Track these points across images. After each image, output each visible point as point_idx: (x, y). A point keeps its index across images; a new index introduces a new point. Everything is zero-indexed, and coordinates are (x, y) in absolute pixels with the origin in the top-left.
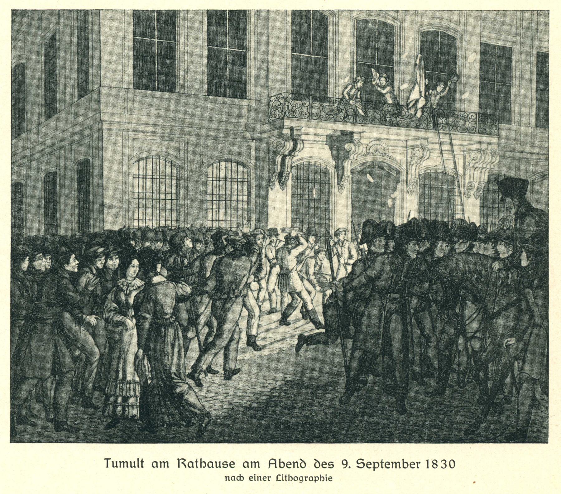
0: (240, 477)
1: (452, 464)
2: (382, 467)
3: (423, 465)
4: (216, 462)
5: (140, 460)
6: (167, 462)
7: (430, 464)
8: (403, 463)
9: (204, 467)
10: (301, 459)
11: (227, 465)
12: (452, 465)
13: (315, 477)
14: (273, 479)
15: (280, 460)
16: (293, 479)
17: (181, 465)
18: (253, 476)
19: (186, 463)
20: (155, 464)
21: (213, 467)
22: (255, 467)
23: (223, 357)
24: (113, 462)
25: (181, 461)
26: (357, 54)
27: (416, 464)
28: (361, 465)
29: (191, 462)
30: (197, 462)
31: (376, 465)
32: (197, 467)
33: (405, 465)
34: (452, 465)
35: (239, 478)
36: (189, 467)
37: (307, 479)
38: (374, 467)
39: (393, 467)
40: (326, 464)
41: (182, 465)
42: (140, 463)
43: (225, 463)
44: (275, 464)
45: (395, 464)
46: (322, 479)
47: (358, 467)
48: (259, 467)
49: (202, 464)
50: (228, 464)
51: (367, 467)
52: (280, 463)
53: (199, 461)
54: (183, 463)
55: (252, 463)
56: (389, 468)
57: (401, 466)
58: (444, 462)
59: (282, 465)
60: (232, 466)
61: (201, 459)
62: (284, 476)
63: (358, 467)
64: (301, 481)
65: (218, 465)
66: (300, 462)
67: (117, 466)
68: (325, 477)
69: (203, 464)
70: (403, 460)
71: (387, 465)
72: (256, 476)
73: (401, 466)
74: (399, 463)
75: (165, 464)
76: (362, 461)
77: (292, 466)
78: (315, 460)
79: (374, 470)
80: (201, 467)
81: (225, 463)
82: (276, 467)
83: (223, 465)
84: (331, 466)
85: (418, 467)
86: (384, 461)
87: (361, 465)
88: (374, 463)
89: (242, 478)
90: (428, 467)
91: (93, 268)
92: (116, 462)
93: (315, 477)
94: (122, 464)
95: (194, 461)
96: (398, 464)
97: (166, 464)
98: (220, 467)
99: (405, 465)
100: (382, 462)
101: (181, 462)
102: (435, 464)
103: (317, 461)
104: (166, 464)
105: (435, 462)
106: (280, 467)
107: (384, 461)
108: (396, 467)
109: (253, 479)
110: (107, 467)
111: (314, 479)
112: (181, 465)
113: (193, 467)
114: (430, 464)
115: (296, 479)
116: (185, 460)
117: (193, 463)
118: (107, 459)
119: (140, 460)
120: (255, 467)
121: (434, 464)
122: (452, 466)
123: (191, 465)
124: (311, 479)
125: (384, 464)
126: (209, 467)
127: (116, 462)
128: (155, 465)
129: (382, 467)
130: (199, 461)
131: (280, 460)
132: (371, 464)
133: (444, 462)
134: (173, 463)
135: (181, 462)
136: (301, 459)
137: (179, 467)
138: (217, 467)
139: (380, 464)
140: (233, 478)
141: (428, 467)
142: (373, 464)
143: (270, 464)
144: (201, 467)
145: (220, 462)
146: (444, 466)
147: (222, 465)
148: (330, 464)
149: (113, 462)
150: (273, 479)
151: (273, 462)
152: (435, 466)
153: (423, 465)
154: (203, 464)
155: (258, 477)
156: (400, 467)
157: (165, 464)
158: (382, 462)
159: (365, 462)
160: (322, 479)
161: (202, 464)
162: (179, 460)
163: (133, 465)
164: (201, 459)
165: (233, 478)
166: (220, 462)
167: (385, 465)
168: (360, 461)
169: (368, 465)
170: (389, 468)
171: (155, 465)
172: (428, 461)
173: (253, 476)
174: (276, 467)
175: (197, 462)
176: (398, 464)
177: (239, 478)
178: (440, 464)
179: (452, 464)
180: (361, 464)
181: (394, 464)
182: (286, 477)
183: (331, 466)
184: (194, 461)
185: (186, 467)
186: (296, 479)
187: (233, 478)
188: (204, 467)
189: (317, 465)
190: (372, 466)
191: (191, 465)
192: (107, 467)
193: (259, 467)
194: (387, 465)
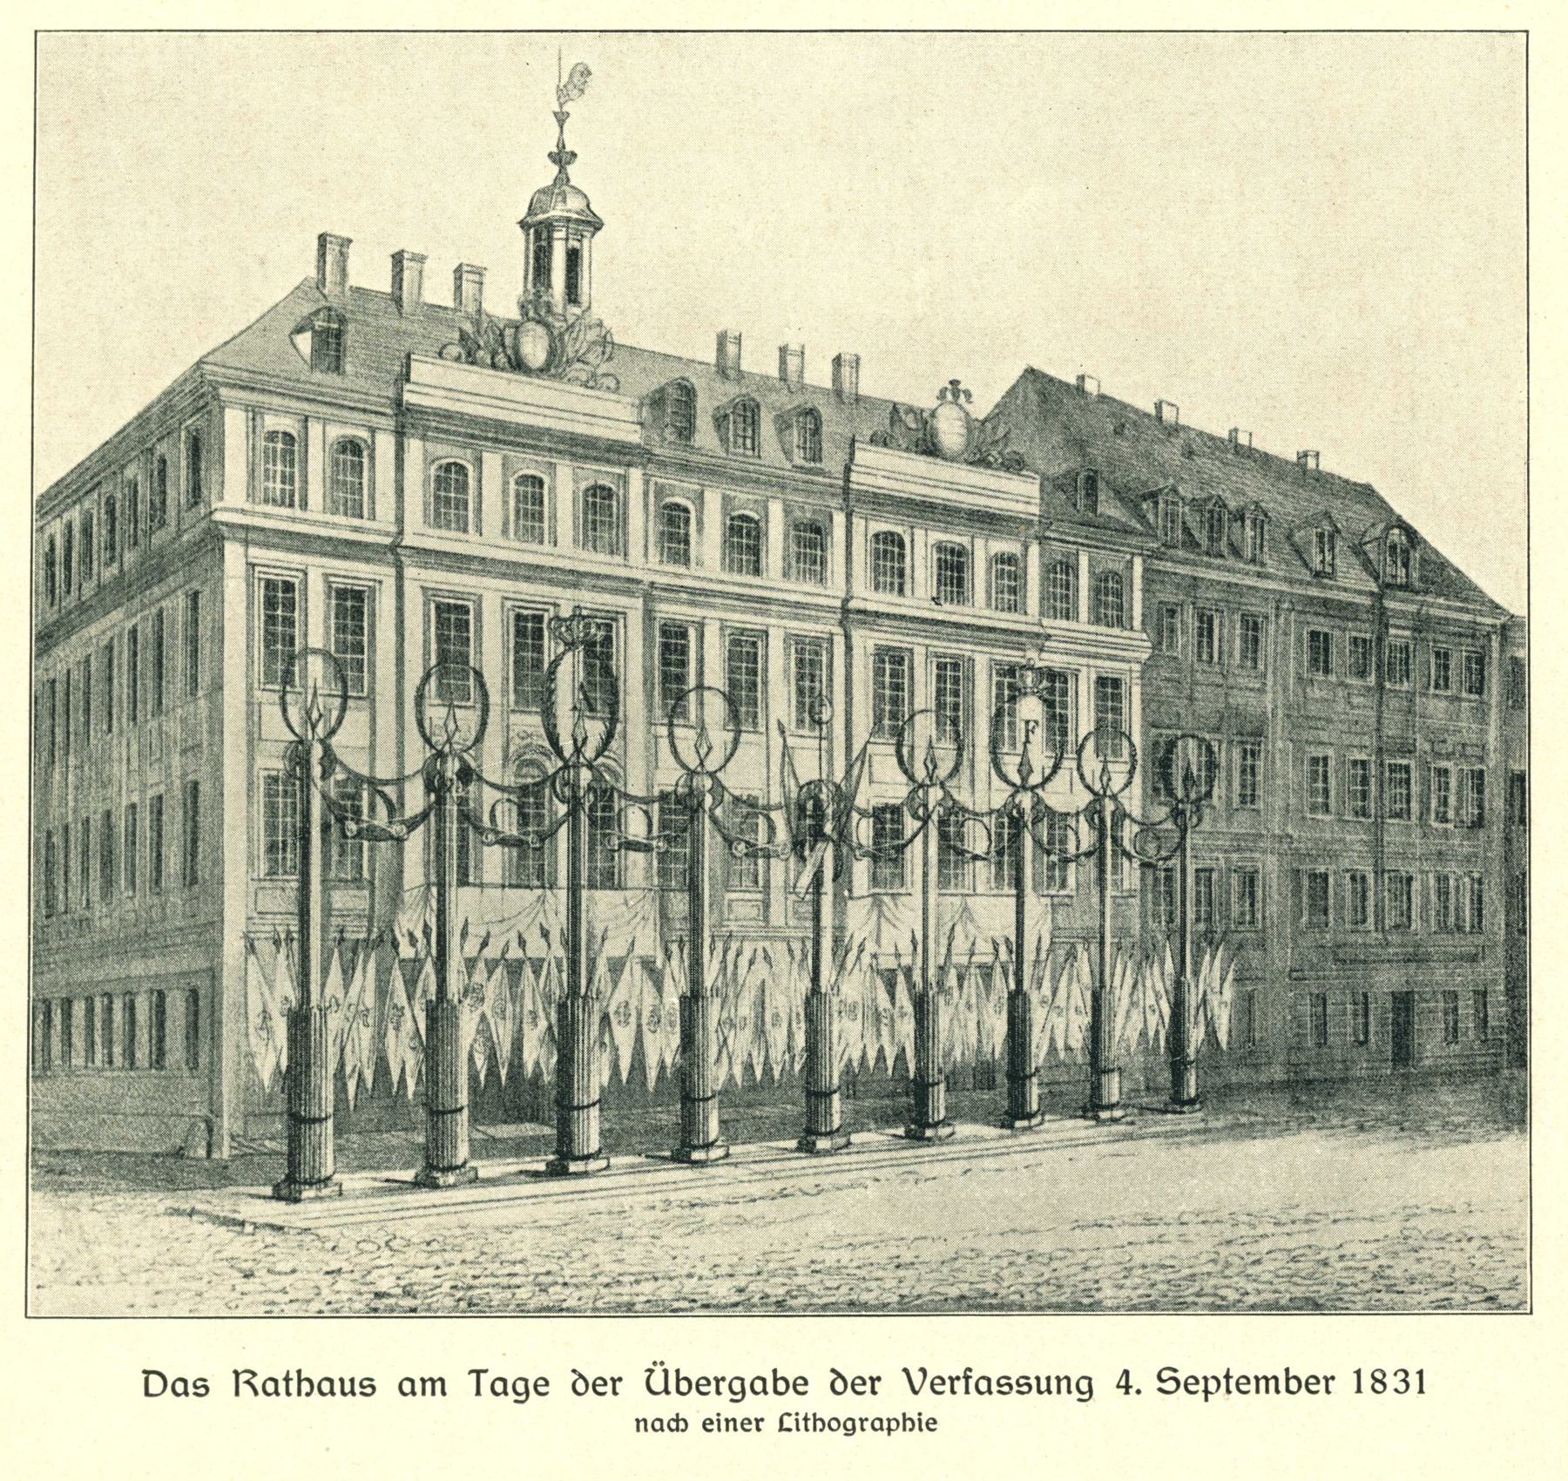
0: (677, 1420)
1: (1414, 1381)
6: (442, 1380)
7: (1367, 1382)
8: (1288, 1380)
9: (308, 1394)
13: (889, 1420)
14: (770, 1425)
15: (678, 1371)
16: (827, 1425)
17: (244, 1388)
18: (714, 1418)
19: (258, 1382)
20: (407, 1387)
22: (1267, 1391)
24: (666, 1372)
25: (244, 1377)
27: (713, 1383)
28: (1171, 1385)
30: (287, 1379)
31: (1212, 1385)
32: (288, 1394)
35: (673, 1425)
37: (867, 1425)
38: (1206, 1392)
39: (1258, 1391)
41: (248, 1387)
43: (366, 1383)
45: (1265, 1383)
46: (909, 1424)
47: (1160, 1390)
48: (444, 1393)
49: (299, 1384)
50: (1013, 1382)
51: (1309, 1391)
52: (678, 1380)
53: (294, 1375)
54: (248, 1382)
56: (1316, 1392)
57: (1282, 1386)
58: (1401, 1375)
59: (684, 1386)
60: (800, 1389)
61: (299, 1372)
62: (801, 1417)
63: (1160, 1390)
64: (850, 1432)
65: (347, 1388)
68: (916, 1418)
69: (305, 1387)
70: (1287, 1370)
72: (722, 1418)
73: (1282, 1386)
74: (1275, 1378)
75: (436, 1385)
76: (1172, 1374)
77: (1252, 1386)
78: (833, 1371)
79: (1206, 1399)
80: (299, 1393)
81: (1022, 1381)
83: (362, 1386)
84: (369, 1390)
85: (615, 1393)
86: (1235, 1374)
87: (1171, 1385)
88: (1206, 1379)
89: (682, 1425)
90: (1359, 1391)
92: (1048, 1379)
93: (889, 1420)
94: (429, 1384)
95: (280, 1377)
96: (1272, 1383)
97: (438, 1385)
98: (353, 1393)
99: (781, 1386)
100: (1227, 1377)
102: (1379, 1381)
103: (840, 1376)
104: (438, 1385)
105: (1379, 1375)
106: (776, 1392)
108: (433, 1393)
109: (715, 1426)
110: (478, 1393)
111: (885, 1425)
112: (244, 1388)
113: (277, 1393)
114: (1367, 1382)
115: (834, 1425)
116: (254, 1374)
117: (412, 1381)
118: (478, 1372)
121: (1377, 1380)
123: (270, 1387)
124: (877, 1424)
125: (1232, 1382)
127: (1048, 1379)
128: (408, 1387)
129: (1228, 1391)
130: (294, 1375)
131: (678, 1371)
132: (1197, 1382)
133: (1401, 1375)
134: (222, 1384)
137: (237, 1393)
138: (343, 1393)
139: (1223, 1382)
140: (657, 1425)
141: (1359, 1391)
142: (1202, 1382)
144: (299, 1393)
145: (352, 1380)
146: (1402, 1387)
147: (358, 1389)
149: (666, 1372)
150: (770, 1425)
152: (1379, 1387)
153: (1340, 1386)
154: (305, 1387)
155: (727, 1421)
156: (1277, 1391)
158: (1227, 1377)
159: (1182, 1377)
160: (909, 1424)
161: (299, 1384)
162: (237, 1373)
164: (299, 1372)
165: (658, 1425)
166: (352, 1380)
167: (1238, 1384)
168: (1165, 1375)
169: (501, 1387)
170: (1316, 1392)
172: (1358, 1372)
173: (714, 1418)
175: (287, 1379)
176: (1272, 1383)
177: (673, 1425)
178: (1393, 1382)
179: (1414, 1381)
180: (1171, 1381)
181: (1262, 1383)
182: (806, 1419)
183: (369, 1390)
184: (280, 1377)
185: (256, 1393)
186: (834, 1425)
187: (657, 1425)
188: (308, 1394)
189: (581, 1386)
190: (1201, 1386)
191: (270, 1387)
192: (478, 1393)
193: (444, 1393)
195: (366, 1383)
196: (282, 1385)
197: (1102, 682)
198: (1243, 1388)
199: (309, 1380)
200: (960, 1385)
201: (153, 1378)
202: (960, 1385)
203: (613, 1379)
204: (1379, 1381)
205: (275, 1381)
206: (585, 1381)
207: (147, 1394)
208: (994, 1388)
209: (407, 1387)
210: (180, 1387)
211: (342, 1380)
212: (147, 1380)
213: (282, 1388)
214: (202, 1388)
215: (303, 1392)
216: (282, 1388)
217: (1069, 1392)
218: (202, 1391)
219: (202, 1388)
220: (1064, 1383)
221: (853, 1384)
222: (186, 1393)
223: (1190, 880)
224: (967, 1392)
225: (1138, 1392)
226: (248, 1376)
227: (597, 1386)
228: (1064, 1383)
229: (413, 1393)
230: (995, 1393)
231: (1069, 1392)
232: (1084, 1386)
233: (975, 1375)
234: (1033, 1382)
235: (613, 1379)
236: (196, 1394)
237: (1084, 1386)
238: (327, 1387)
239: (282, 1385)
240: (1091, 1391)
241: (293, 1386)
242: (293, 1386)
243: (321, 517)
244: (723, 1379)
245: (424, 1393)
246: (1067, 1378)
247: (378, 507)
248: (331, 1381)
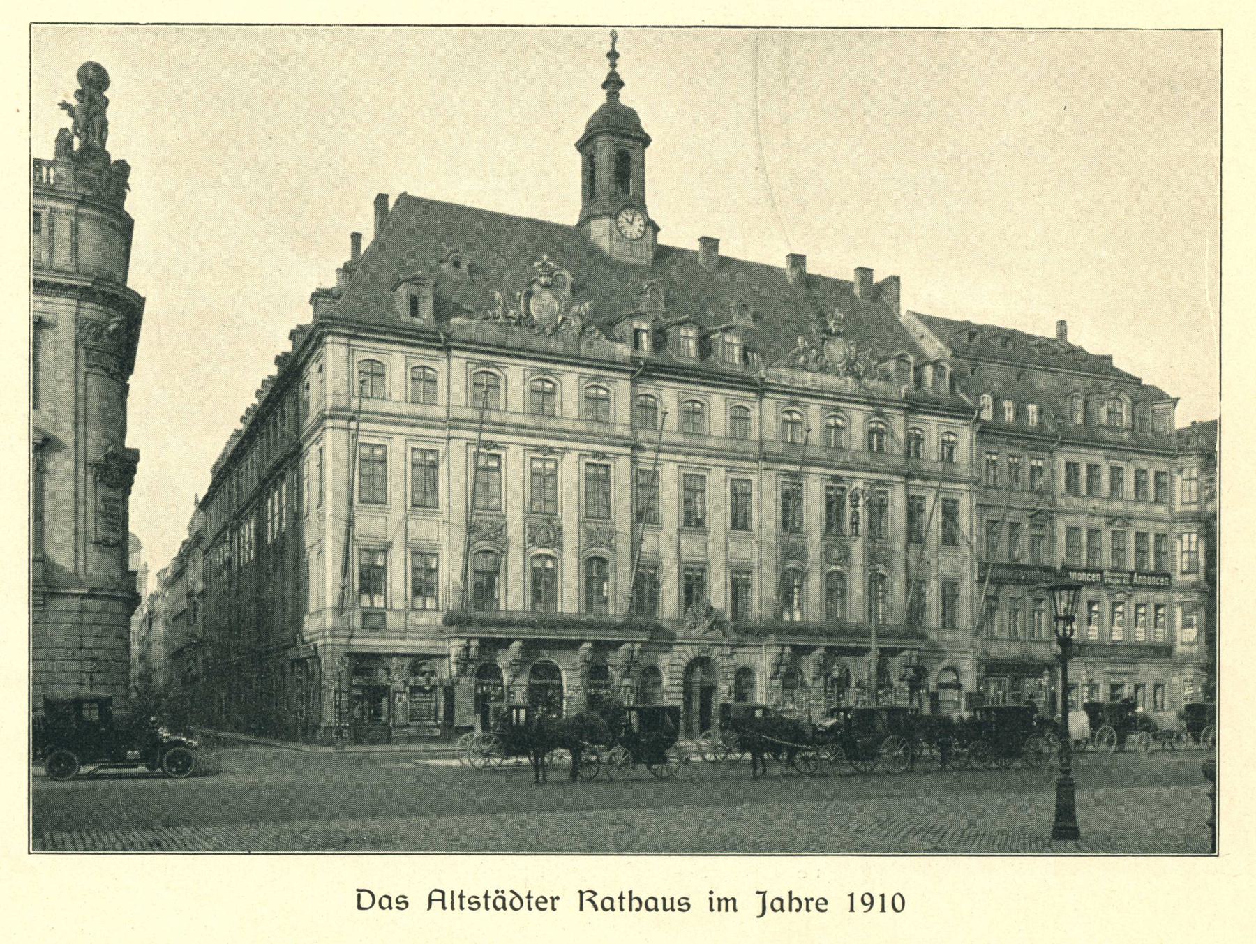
1: (898, 904)
2: (530, 909)
4: (664, 899)
5: (456, 894)
8: (791, 900)
9: (637, 910)
12: (898, 905)
17: (587, 905)
19: (597, 900)
21: (613, 909)
22: (727, 910)
23: (1195, 635)
27: (550, 901)
30: (621, 898)
32: (622, 909)
34: (898, 905)
41: (590, 904)
42: (457, 901)
44: (443, 900)
48: (735, 910)
49: (632, 901)
53: (626, 895)
54: (590, 900)
56: (545, 909)
61: (631, 892)
65: (668, 906)
69: (635, 904)
70: (790, 893)
75: (729, 903)
78: (758, 893)
82: (444, 908)
83: (679, 903)
84: (685, 907)
85: (554, 909)
86: (535, 895)
90: (852, 910)
94: (723, 903)
97: (731, 903)
98: (673, 909)
100: (529, 897)
101: (586, 898)
104: (731, 903)
107: (535, 895)
112: (587, 905)
116: (595, 894)
119: (456, 894)
120: (727, 910)
122: (899, 906)
123: (607, 904)
125: (465, 901)
126: (383, 908)
130: (626, 895)
132: (546, 901)
135: (586, 898)
137: (581, 909)
138: (665, 909)
141: (852, 910)
143: (430, 900)
144: (790, 909)
145: (672, 899)
147: (676, 906)
151: (437, 895)
154: (635, 904)
157: (729, 903)
158: (529, 897)
161: (632, 901)
162: (581, 893)
164: (631, 892)
166: (672, 899)
167: (537, 902)
170: (545, 909)
172: (852, 896)
174: (444, 908)
175: (621, 898)
179: (898, 904)
185: (596, 909)
188: (637, 910)
191: (607, 904)
193: (735, 910)
195: (683, 901)
197: (1068, 464)
198: (541, 905)
199: (638, 899)
201: (363, 894)
203: (552, 898)
207: (360, 907)
208: (394, 904)
210: (385, 902)
211: (664, 899)
212: (359, 896)
214: (403, 903)
215: (794, 909)
218: (685, 907)
219: (403, 903)
222: (390, 907)
226: (590, 895)
230: (677, 911)
234: (465, 904)
235: (552, 898)
236: (680, 910)
238: (652, 905)
241: (626, 903)
242: (626, 903)
243: (406, 409)
244: (812, 899)
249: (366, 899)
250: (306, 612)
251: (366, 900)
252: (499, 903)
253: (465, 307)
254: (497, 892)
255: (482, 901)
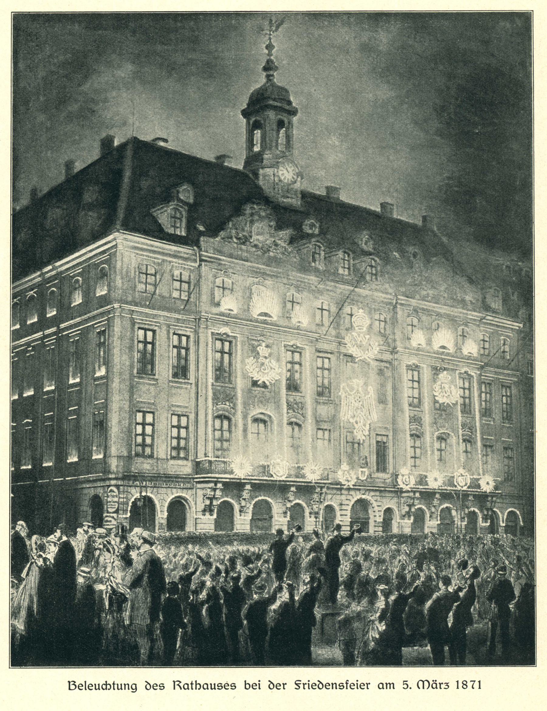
3: (453, 685)
4: (211, 684)
6: (393, 684)
7: (460, 685)
9: (199, 689)
10: (319, 681)
11: (222, 687)
17: (177, 687)
19: (181, 685)
20: (381, 686)
21: (208, 689)
22: (390, 688)
25: (72, 683)
26: (108, 305)
27: (366, 685)
29: (381, 683)
32: (192, 689)
33: (198, 686)
36: (103, 689)
39: (333, 688)
40: (228, 685)
41: (178, 687)
48: (394, 688)
50: (223, 685)
53: (194, 682)
54: (178, 685)
55: (386, 684)
56: (228, 689)
61: (196, 681)
65: (213, 687)
66: (317, 683)
67: (121, 689)
70: (245, 681)
71: (89, 687)
75: (391, 685)
77: (331, 687)
78: (269, 681)
80: (196, 689)
81: (219, 685)
83: (218, 686)
85: (368, 688)
91: (271, 102)
92: (121, 685)
94: (388, 685)
95: (189, 683)
97: (392, 685)
98: (215, 689)
100: (114, 684)
101: (177, 684)
102: (465, 685)
103: (272, 683)
104: (392, 685)
105: (465, 683)
107: (359, 683)
110: (458, 688)
112: (177, 687)
113: (188, 689)
114: (460, 685)
116: (180, 682)
120: (390, 688)
121: (465, 685)
123: (186, 686)
125: (349, 685)
126: (204, 689)
127: (121, 685)
128: (381, 686)
129: (114, 689)
130: (194, 682)
132: (92, 686)
135: (177, 684)
136: (319, 681)
137: (174, 689)
138: (118, 689)
139: (112, 686)
144: (196, 689)
145: (215, 684)
147: (216, 687)
148: (233, 685)
152: (465, 687)
154: (198, 686)
157: (391, 685)
158: (114, 684)
162: (174, 682)
163: (120, 687)
164: (196, 681)
166: (215, 684)
167: (350, 686)
169: (154, 687)
170: (228, 689)
171: (381, 686)
172: (458, 682)
178: (470, 684)
183: (234, 688)
184: (189, 683)
185: (181, 689)
188: (199, 689)
191: (186, 686)
193: (394, 688)
194: (89, 687)
196: (190, 686)
200: (306, 686)
202: (306, 686)
203: (283, 684)
204: (465, 685)
205: (188, 684)
206: (323, 685)
209: (381, 686)
211: (211, 684)
213: (190, 687)
216: (190, 687)
217: (129, 689)
219: (162, 687)
220: (127, 686)
221: (153, 686)
223: (298, 480)
224: (309, 688)
225: (410, 688)
226: (178, 683)
227: (277, 686)
228: (127, 686)
229: (383, 688)
230: (217, 690)
231: (129, 689)
232: (134, 687)
233: (350, 683)
235: (283, 684)
236: (218, 689)
237: (134, 687)
239: (190, 686)
240: (136, 689)
241: (194, 686)
242: (194, 686)
245: (387, 688)
246: (336, 684)
247: (323, 319)
248: (207, 684)
249: (72, 685)
250: (73, 547)
251: (247, 686)
252: (434, 686)
253: (158, 288)
254: (433, 681)
255: (345, 685)
